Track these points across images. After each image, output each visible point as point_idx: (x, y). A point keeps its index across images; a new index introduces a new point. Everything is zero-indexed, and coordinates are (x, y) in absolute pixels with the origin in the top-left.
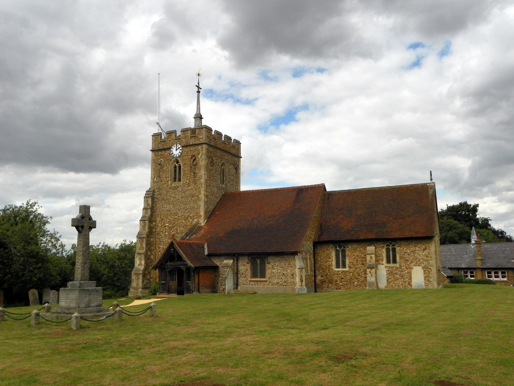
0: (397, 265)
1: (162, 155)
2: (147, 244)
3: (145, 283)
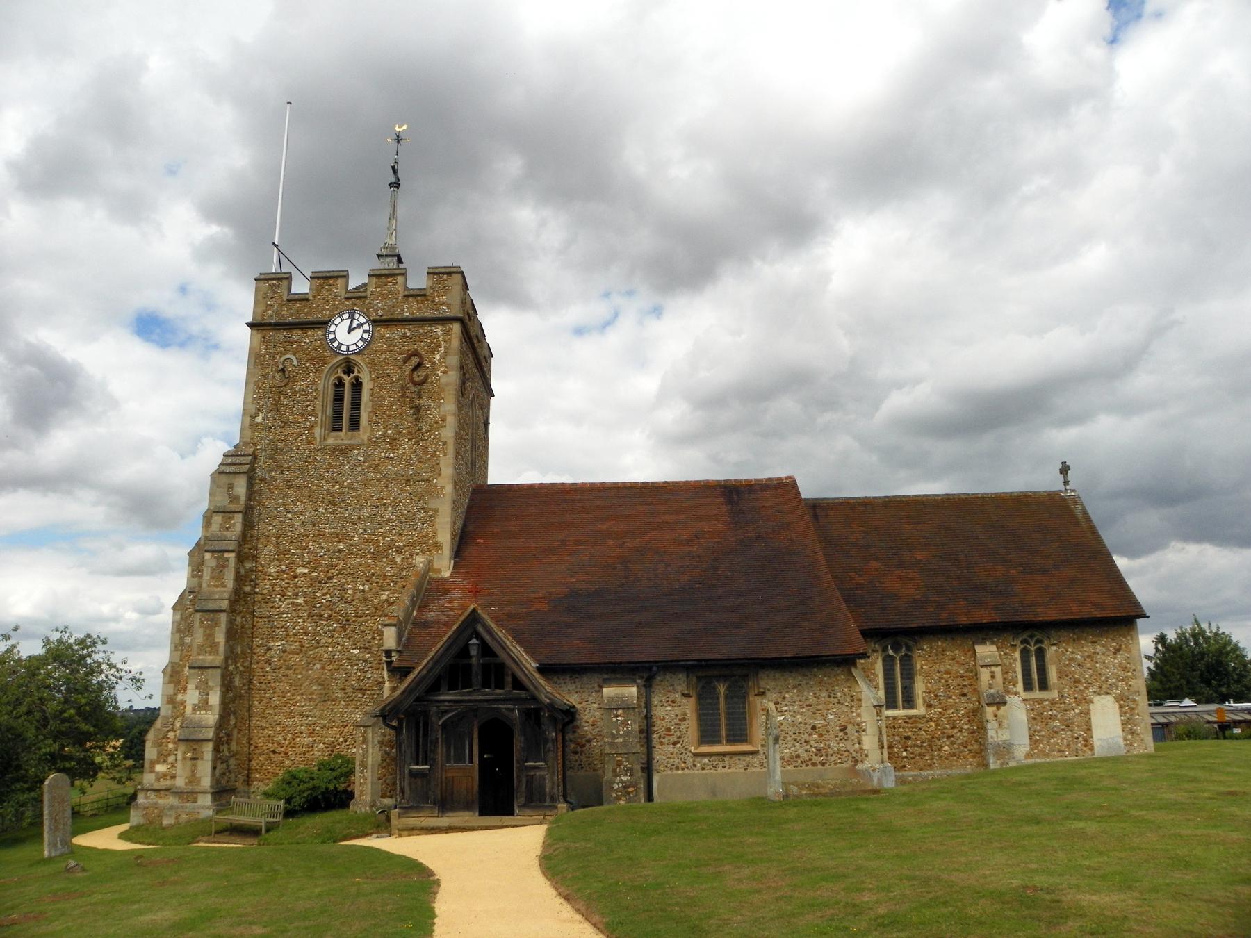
0: (1054, 694)
1: (292, 343)
2: (231, 634)
3: (217, 772)
